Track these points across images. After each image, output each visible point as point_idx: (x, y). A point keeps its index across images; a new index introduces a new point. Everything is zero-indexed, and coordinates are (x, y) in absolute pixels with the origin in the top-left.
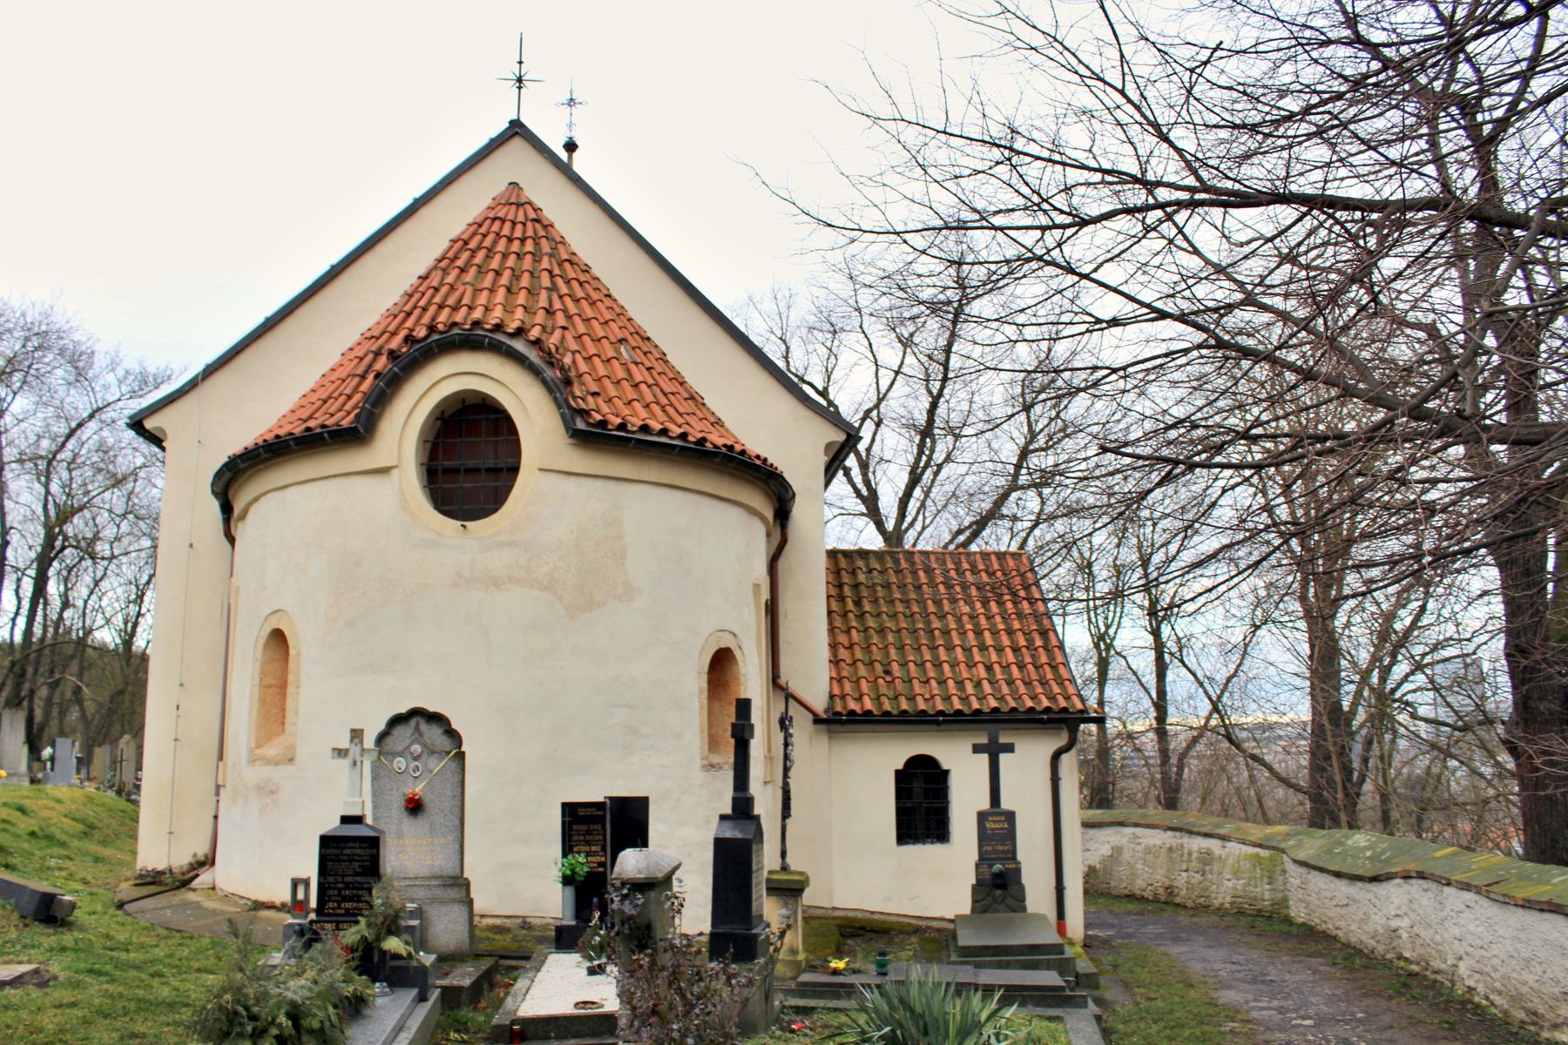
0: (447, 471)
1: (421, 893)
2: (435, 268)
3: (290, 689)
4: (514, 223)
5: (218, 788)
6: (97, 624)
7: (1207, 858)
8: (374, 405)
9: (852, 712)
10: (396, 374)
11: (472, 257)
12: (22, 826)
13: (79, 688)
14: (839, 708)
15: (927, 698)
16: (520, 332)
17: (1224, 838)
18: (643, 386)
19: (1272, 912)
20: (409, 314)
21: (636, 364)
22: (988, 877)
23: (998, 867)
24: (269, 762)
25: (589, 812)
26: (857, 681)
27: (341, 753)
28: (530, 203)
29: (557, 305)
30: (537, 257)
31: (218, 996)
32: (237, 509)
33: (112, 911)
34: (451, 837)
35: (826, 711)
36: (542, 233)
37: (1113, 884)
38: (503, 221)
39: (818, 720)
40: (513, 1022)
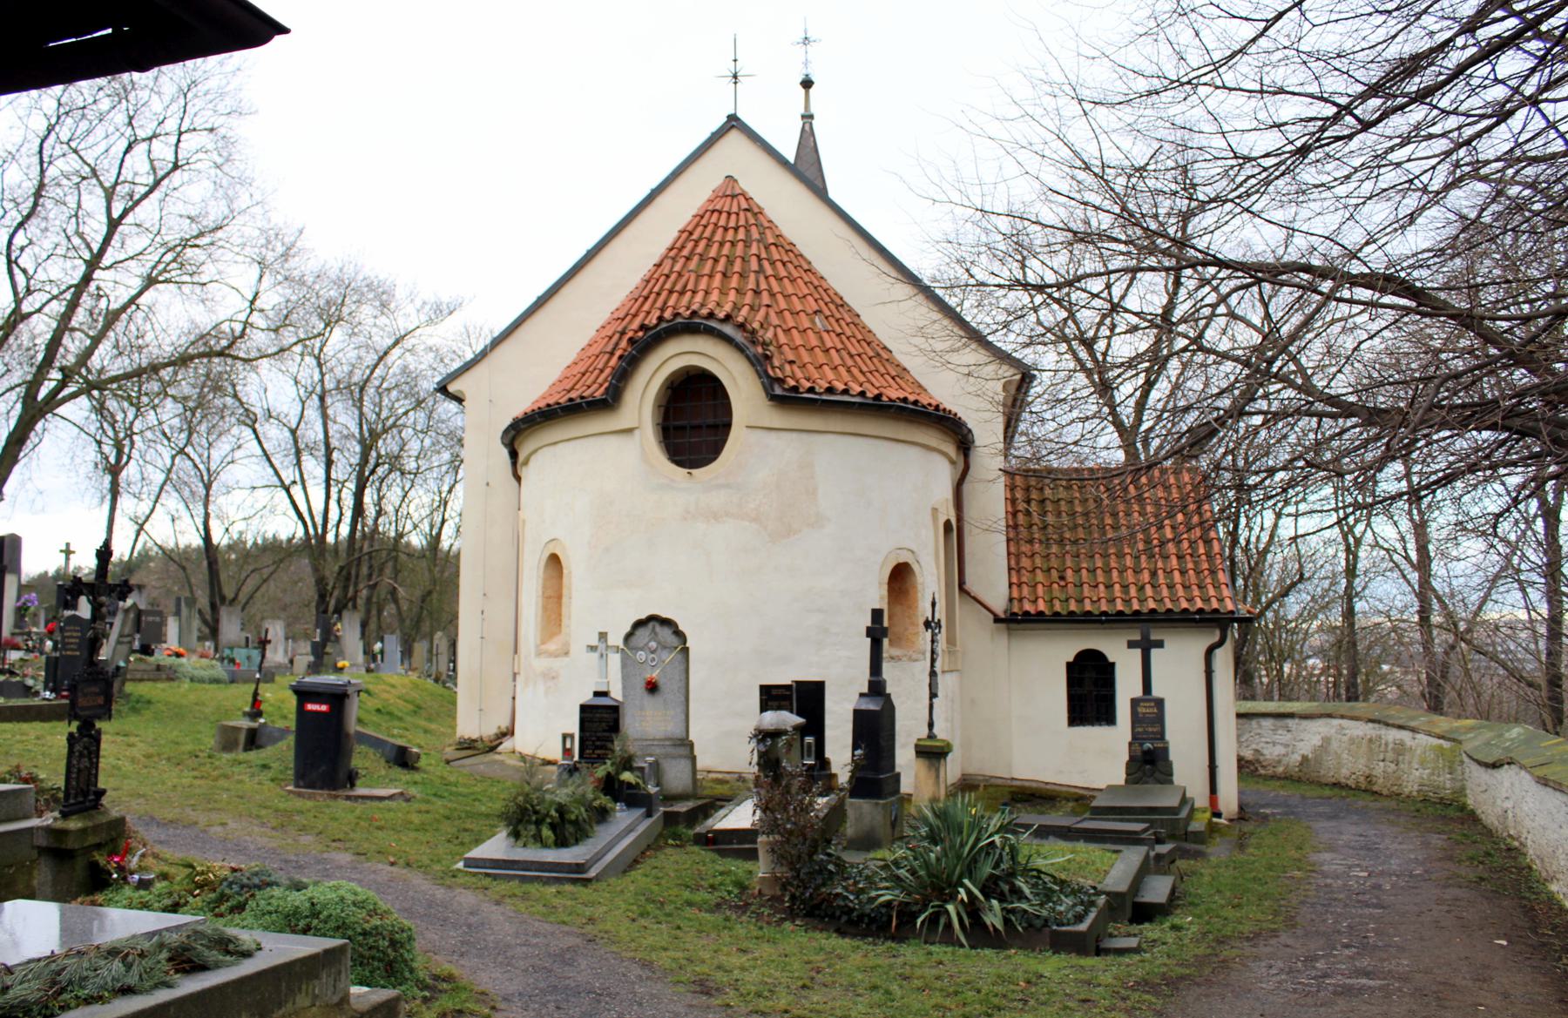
0: (676, 428)
1: (658, 751)
2: (666, 257)
3: (564, 600)
4: (729, 214)
5: (515, 675)
6: (406, 530)
7: (1400, 750)
8: (619, 381)
9: (1027, 613)
10: (634, 356)
11: (696, 246)
12: (369, 704)
13: (395, 588)
14: (1016, 610)
15: (1095, 600)
16: (728, 318)
17: (1413, 730)
18: (833, 352)
19: (1453, 800)
20: (646, 298)
21: (828, 332)
22: (1139, 753)
23: (1148, 745)
24: (555, 655)
25: (780, 692)
26: (1035, 586)
27: (592, 648)
28: (743, 194)
29: (763, 286)
30: (747, 244)
31: (515, 798)
32: (521, 457)
33: (442, 764)
34: (680, 710)
35: (1005, 612)
36: (752, 221)
37: (1322, 772)
38: (720, 212)
39: (997, 620)
40: (708, 832)
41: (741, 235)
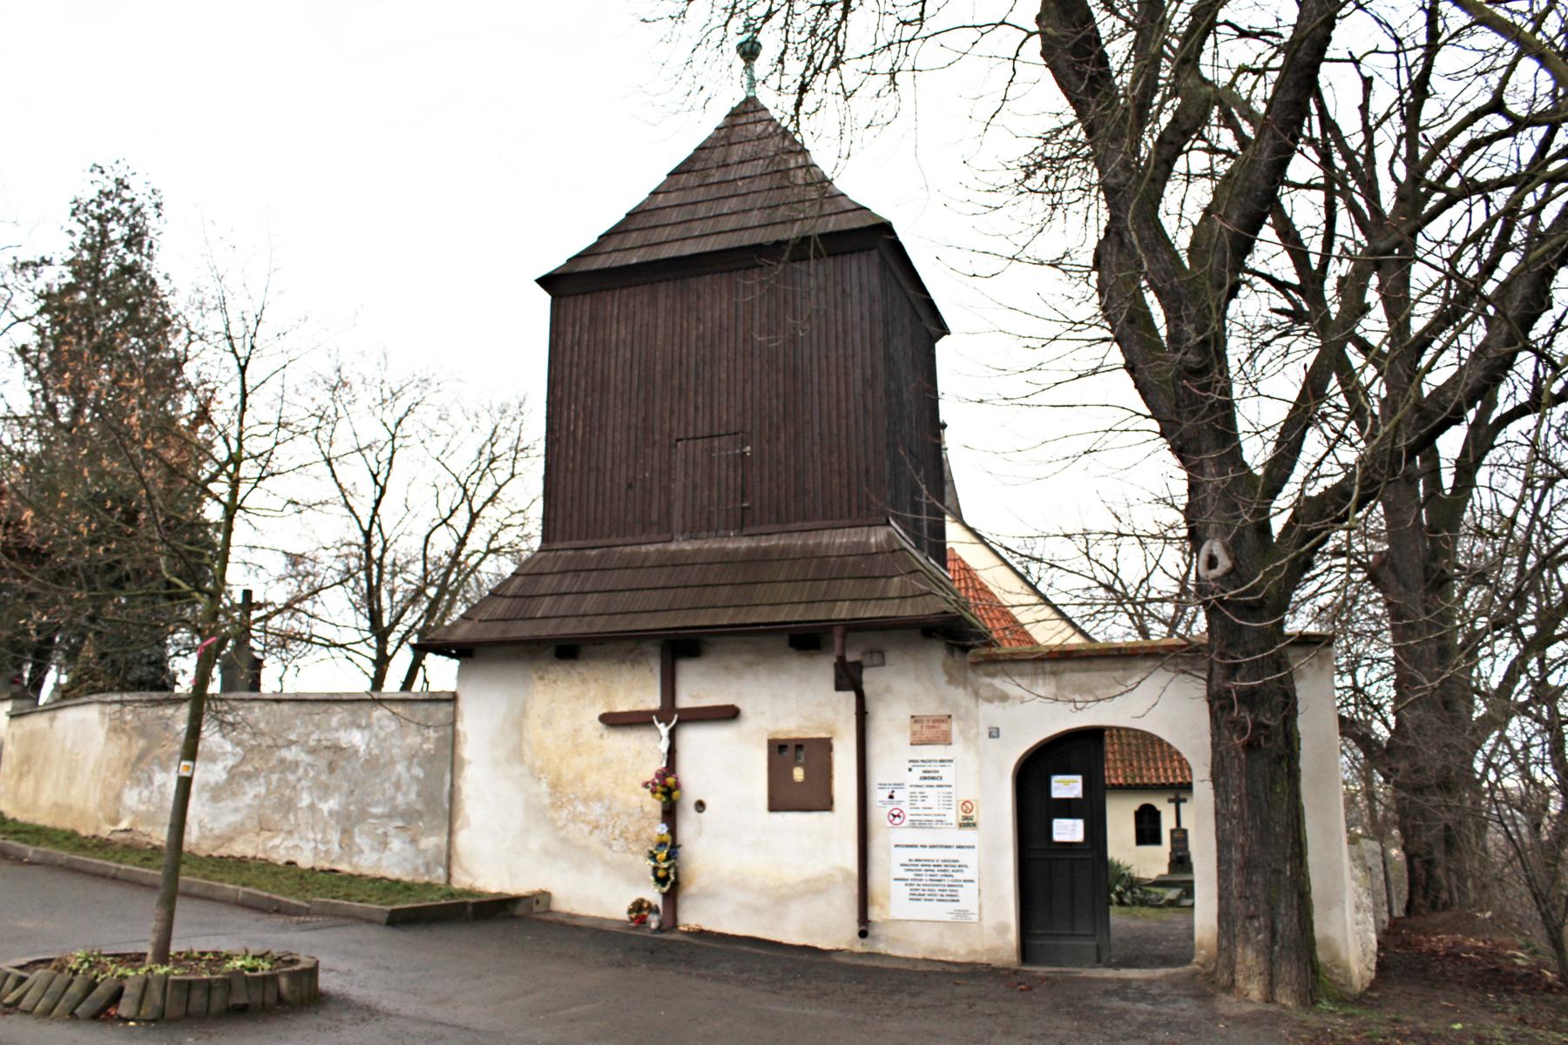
15: (1149, 777)
30: (967, 589)
41: (963, 585)
